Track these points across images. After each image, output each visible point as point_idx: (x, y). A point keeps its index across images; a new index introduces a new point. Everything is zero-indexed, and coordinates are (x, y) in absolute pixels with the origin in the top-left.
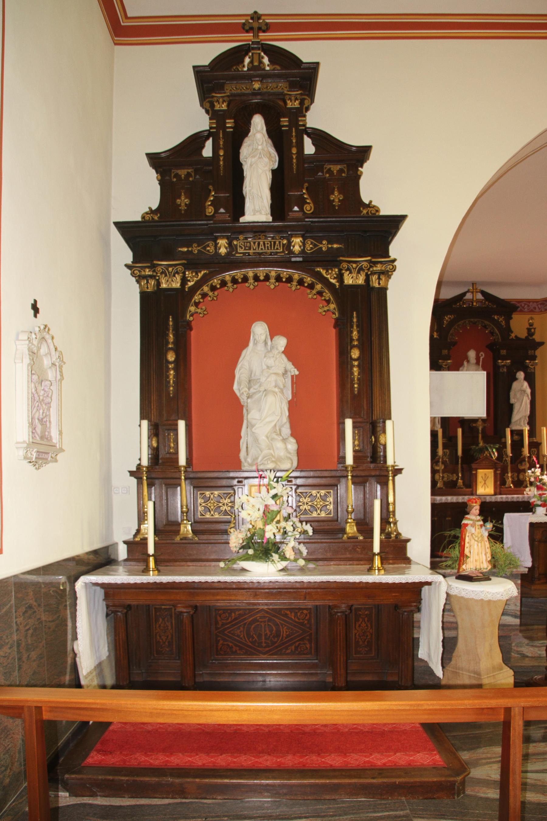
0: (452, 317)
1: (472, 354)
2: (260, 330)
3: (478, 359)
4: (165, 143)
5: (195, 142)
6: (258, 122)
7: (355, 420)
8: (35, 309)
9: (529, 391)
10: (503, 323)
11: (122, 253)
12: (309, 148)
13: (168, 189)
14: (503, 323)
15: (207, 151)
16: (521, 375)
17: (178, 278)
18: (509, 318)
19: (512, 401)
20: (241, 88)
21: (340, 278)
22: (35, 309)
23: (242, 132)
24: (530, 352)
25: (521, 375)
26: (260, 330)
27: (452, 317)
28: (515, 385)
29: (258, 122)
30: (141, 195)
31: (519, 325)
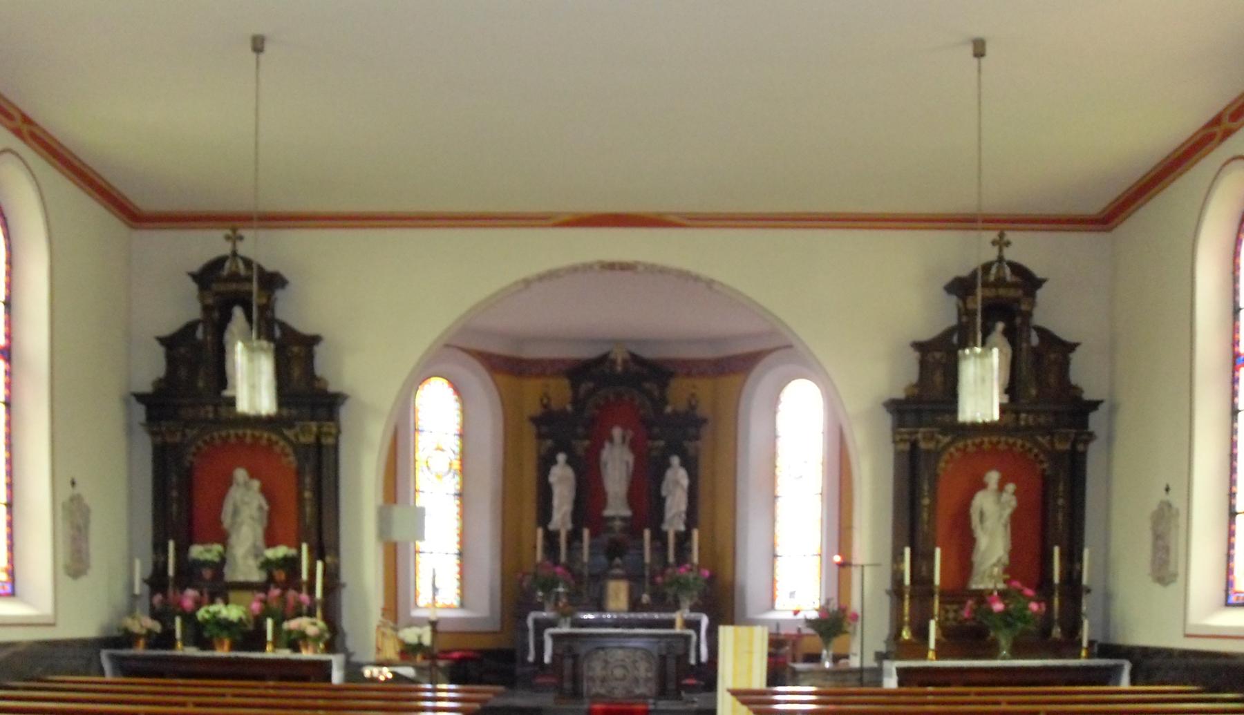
0: (591, 385)
1: (617, 432)
2: (241, 474)
3: (624, 438)
4: (168, 329)
5: (190, 328)
6: (238, 312)
7: (947, 418)
8: (73, 483)
9: (685, 481)
10: (656, 393)
11: (140, 411)
12: (1035, 340)
13: (171, 361)
14: (656, 393)
15: (199, 334)
16: (675, 460)
17: (179, 434)
18: (664, 385)
19: (664, 493)
20: (221, 287)
21: (1052, 443)
22: (73, 483)
23: (226, 318)
24: (692, 431)
25: (675, 460)
26: (241, 474)
27: (591, 385)
28: (669, 474)
29: (238, 312)
30: (150, 368)
31: (679, 393)
